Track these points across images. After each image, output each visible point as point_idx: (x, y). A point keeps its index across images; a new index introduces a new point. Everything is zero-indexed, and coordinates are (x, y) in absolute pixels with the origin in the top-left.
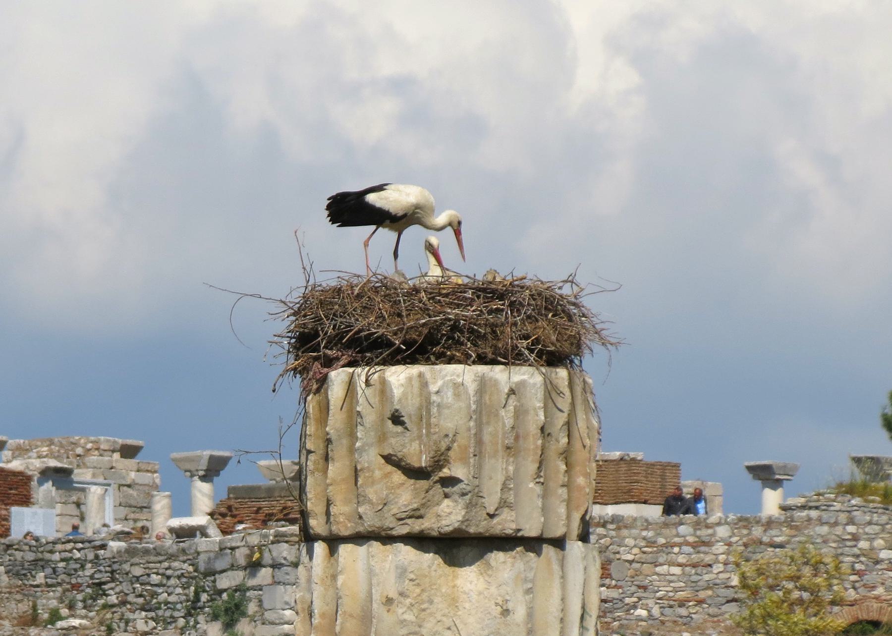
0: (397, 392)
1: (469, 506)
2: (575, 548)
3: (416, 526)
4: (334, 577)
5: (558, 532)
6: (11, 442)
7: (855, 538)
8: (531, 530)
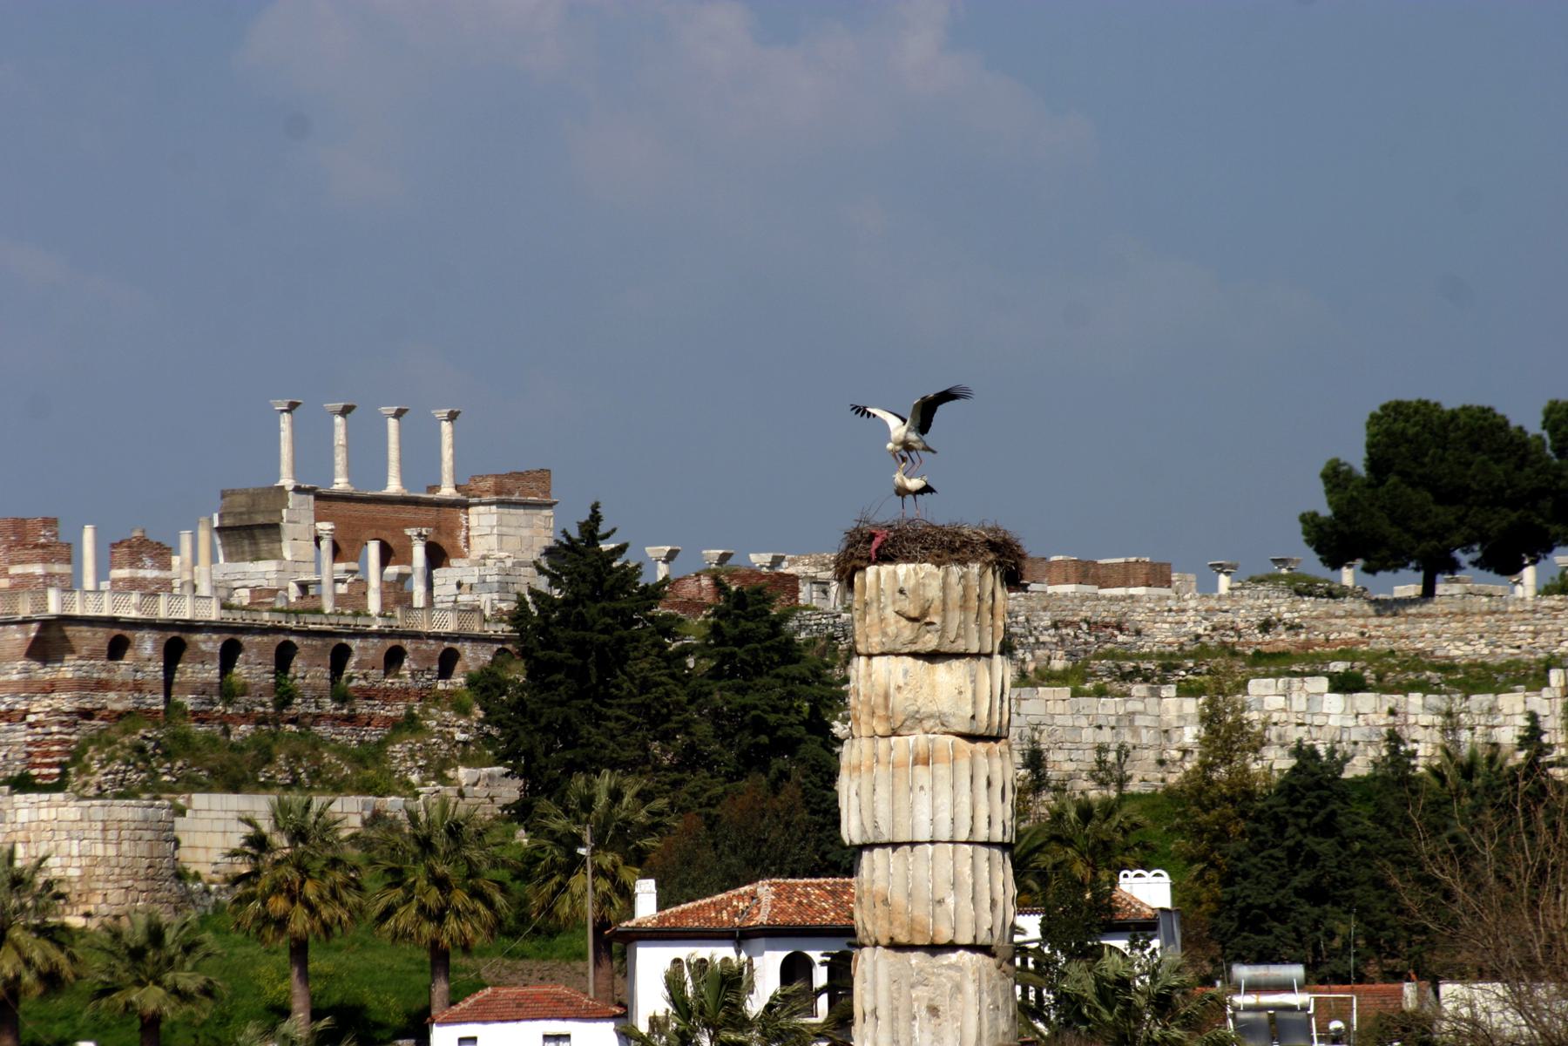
0: (901, 578)
1: (941, 637)
3: (914, 648)
5: (989, 650)
7: (1270, 606)
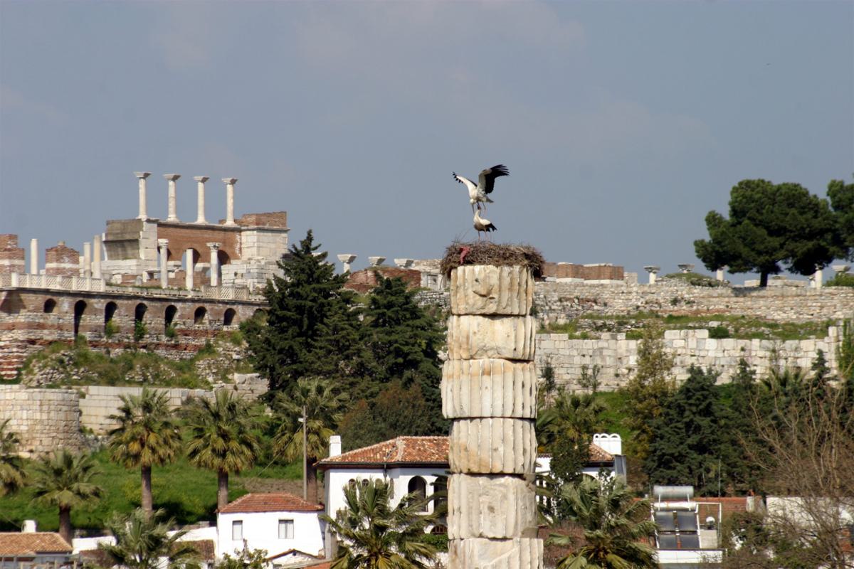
0: (477, 273)
1: (498, 306)
2: (529, 317)
4: (459, 326)
5: (524, 313)
6: (415, 261)
7: (677, 291)
8: (516, 312)
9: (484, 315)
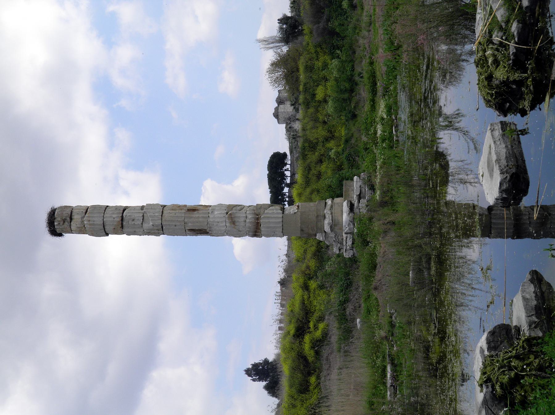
9: (71, 222)
